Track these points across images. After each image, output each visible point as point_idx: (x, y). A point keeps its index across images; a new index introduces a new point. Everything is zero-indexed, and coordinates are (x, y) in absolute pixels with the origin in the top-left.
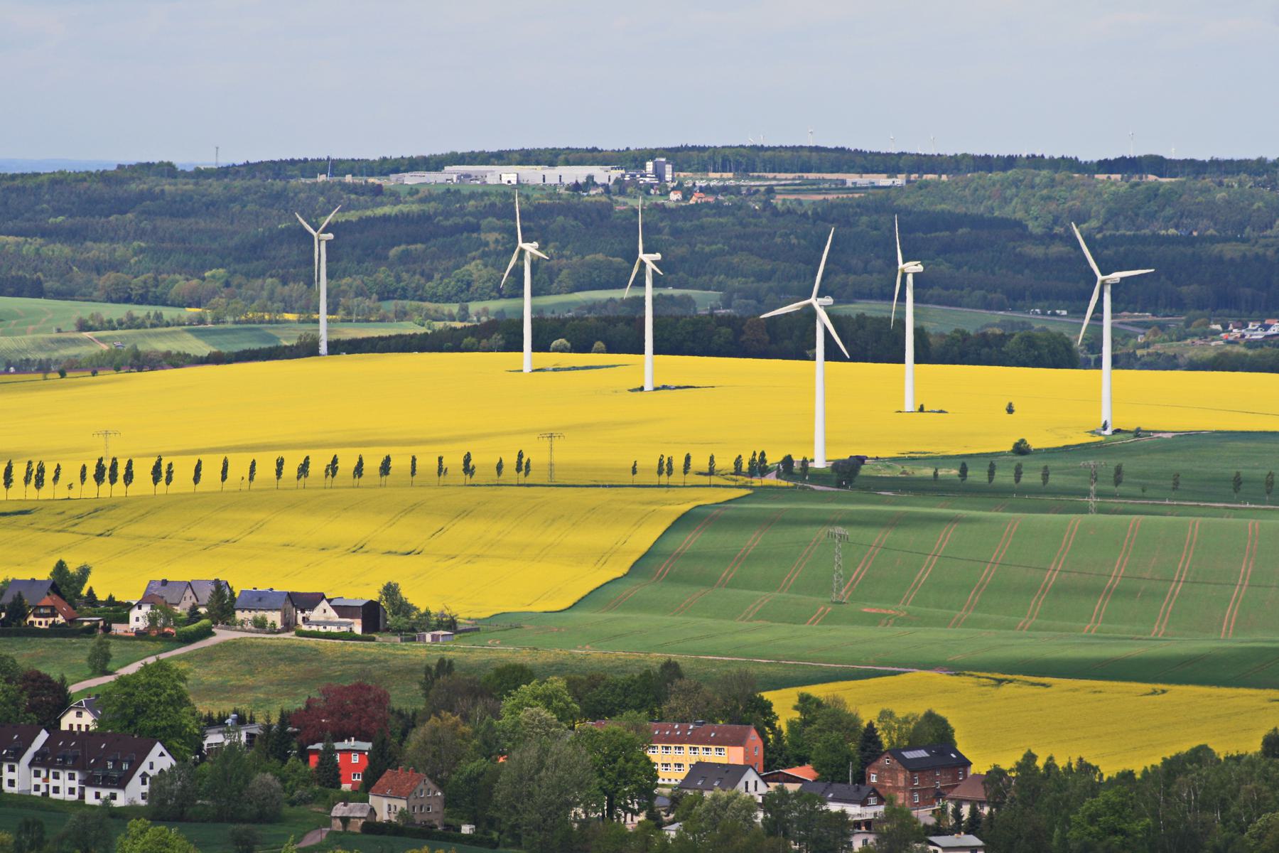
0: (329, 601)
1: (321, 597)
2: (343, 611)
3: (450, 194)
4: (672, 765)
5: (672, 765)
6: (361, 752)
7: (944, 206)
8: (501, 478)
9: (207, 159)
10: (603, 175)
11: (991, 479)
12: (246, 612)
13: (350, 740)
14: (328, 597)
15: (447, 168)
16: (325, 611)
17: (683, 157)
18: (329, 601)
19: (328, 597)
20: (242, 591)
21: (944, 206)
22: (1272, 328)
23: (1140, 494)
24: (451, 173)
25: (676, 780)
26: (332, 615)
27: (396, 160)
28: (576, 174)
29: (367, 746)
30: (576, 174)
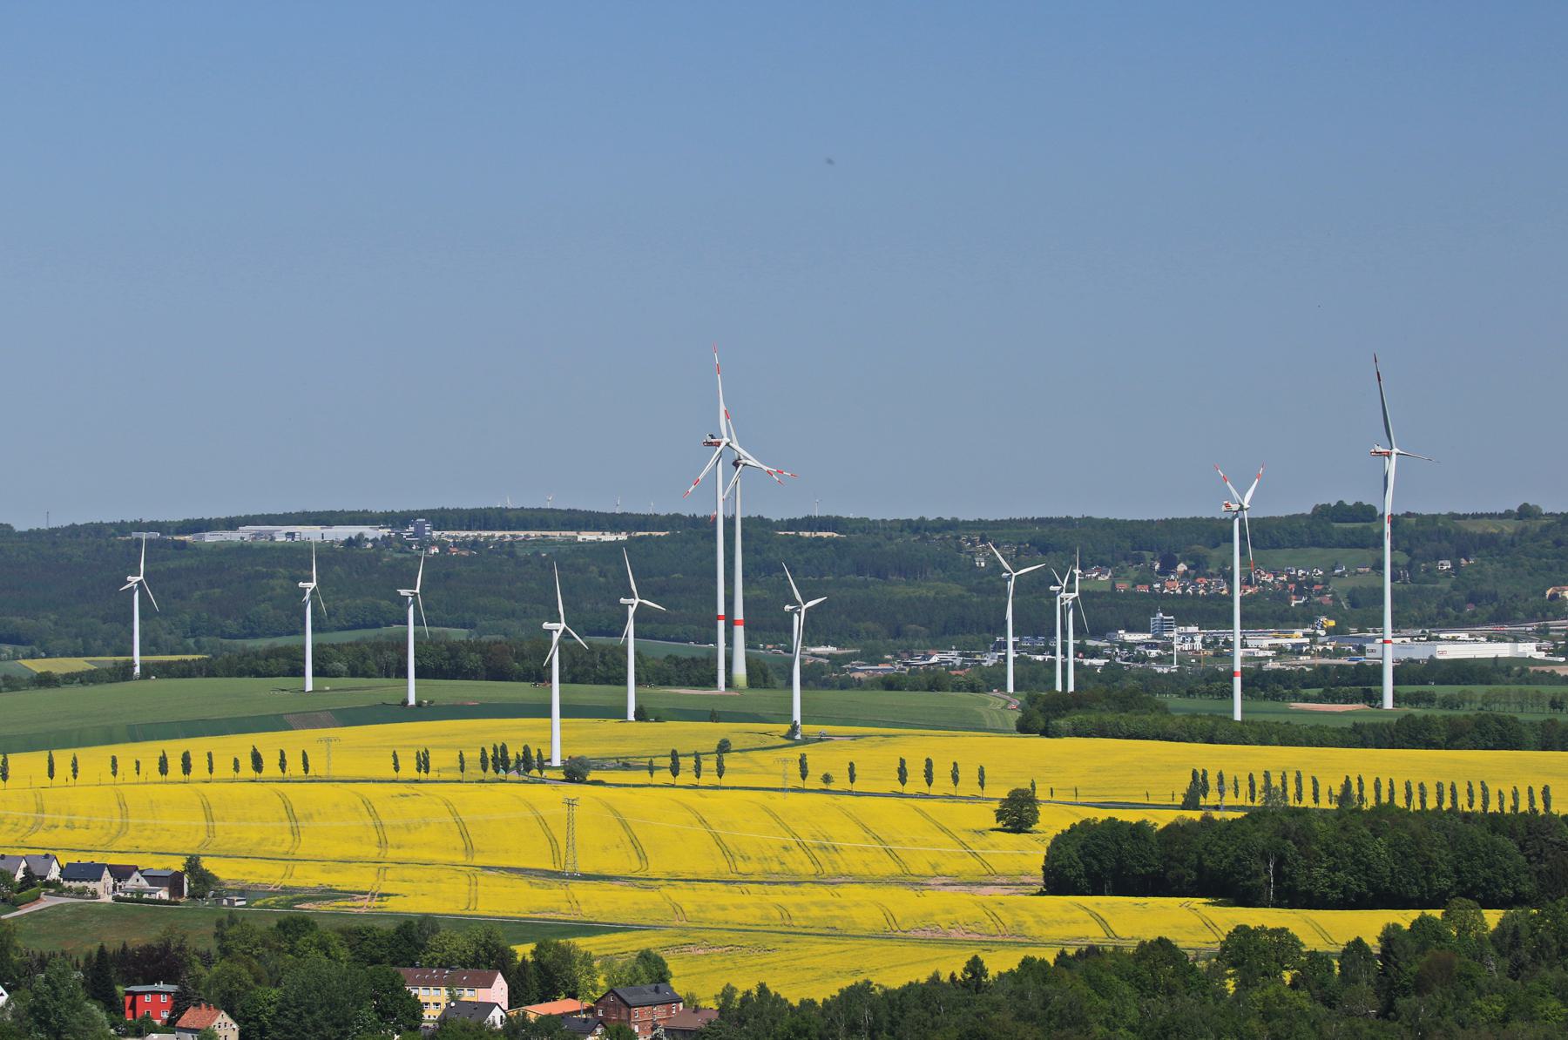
0: (141, 872)
1: (136, 868)
2: (154, 879)
3: (242, 550)
4: (432, 1004)
5: (432, 1004)
6: (168, 993)
7: (18, 620)
8: (308, 775)
9: (40, 523)
10: (370, 532)
11: (50, 752)
12: (78, 882)
13: (159, 983)
14: (140, 869)
15: (240, 528)
16: (138, 880)
17: (442, 519)
18: (141, 872)
19: (140, 869)
20: (68, 864)
21: (18, 620)
22: (933, 658)
23: (1073, 799)
24: (244, 534)
25: (435, 1017)
26: (144, 883)
27: (198, 520)
28: (352, 531)
29: (172, 988)
30: (352, 531)
